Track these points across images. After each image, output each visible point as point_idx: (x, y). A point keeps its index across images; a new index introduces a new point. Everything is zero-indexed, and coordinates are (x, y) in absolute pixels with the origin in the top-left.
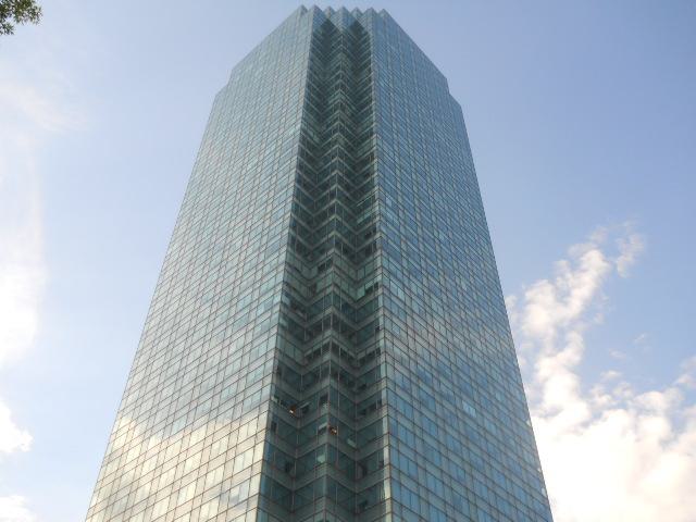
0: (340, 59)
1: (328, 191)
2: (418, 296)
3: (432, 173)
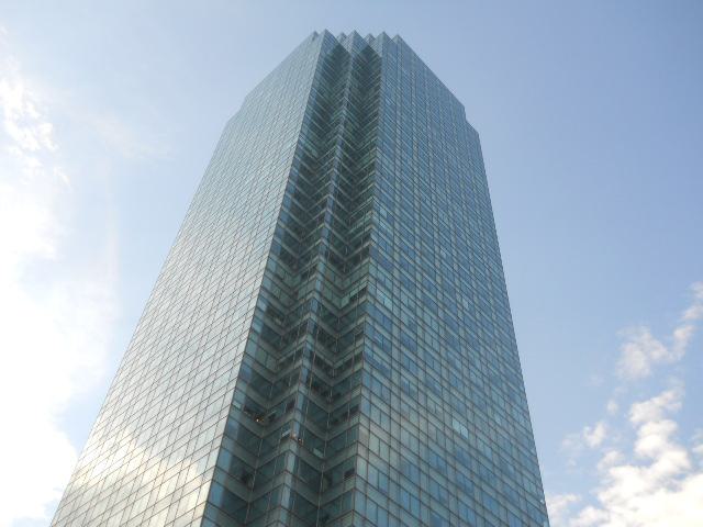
0: (349, 79)
1: (360, 249)
2: (409, 308)
3: (438, 190)
